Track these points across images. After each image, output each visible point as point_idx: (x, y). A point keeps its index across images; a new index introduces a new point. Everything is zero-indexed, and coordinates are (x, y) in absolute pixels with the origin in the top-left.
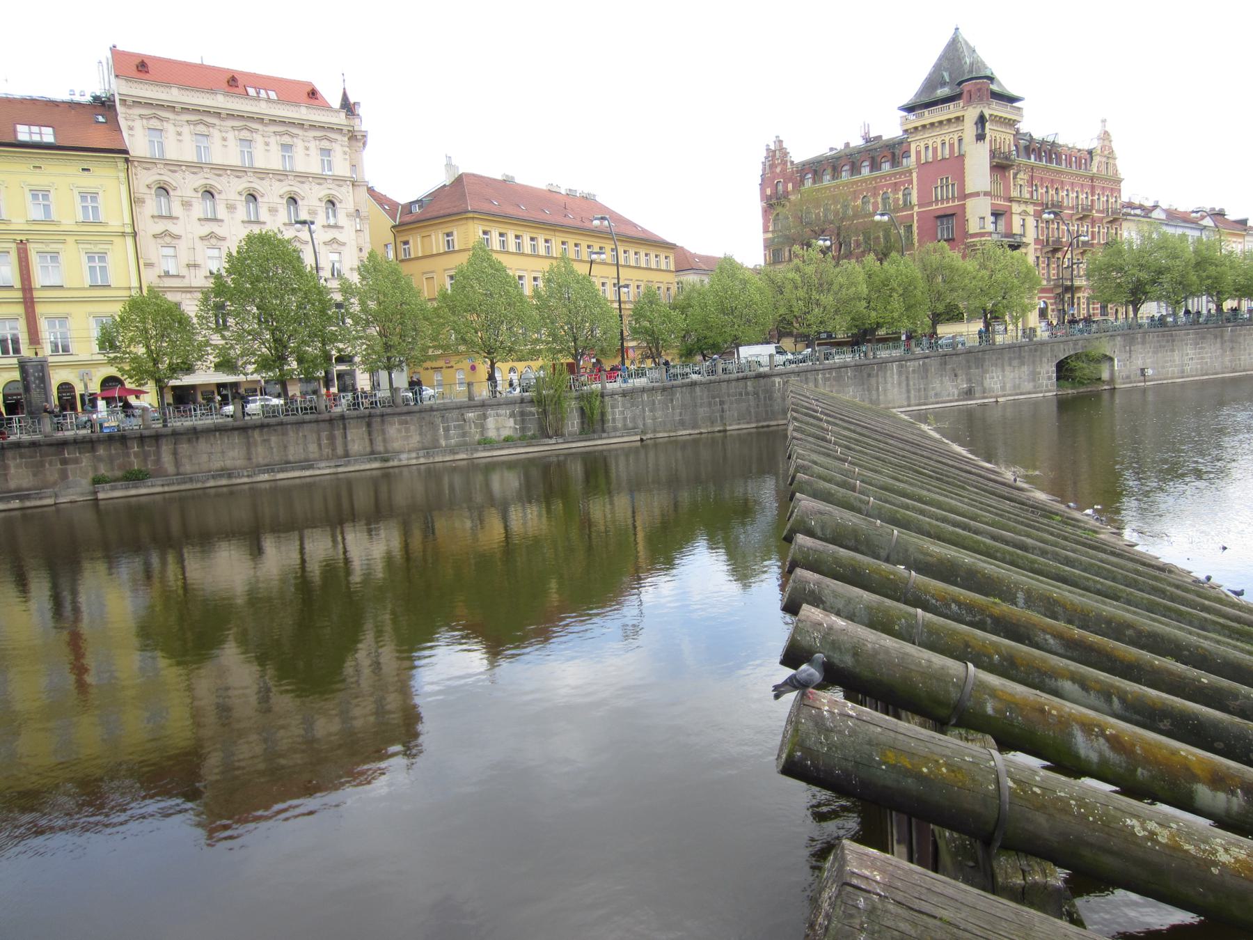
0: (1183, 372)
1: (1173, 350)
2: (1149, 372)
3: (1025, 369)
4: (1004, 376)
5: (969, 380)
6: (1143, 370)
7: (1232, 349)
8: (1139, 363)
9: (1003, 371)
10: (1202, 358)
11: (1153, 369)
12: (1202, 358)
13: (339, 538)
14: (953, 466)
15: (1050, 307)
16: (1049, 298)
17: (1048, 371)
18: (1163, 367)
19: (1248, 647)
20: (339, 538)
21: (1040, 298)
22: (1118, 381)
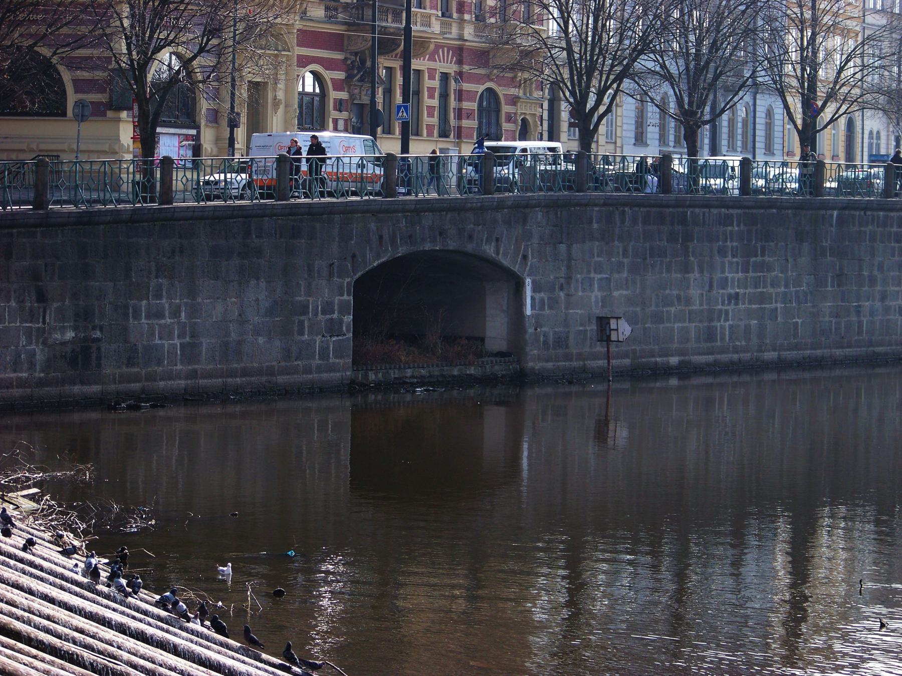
0: (710, 335)
1: (686, 269)
2: (623, 329)
3: (259, 294)
4: (194, 311)
5: (84, 317)
6: (603, 323)
7: (840, 278)
8: (590, 298)
9: (192, 293)
10: (762, 298)
11: (632, 321)
12: (762, 298)
13: (493, 121)
14: (122, 629)
15: (334, 95)
16: (329, 64)
17: (330, 299)
18: (658, 318)
19: (6, 619)
20: (493, 121)
21: (303, 62)
22: (533, 352)
